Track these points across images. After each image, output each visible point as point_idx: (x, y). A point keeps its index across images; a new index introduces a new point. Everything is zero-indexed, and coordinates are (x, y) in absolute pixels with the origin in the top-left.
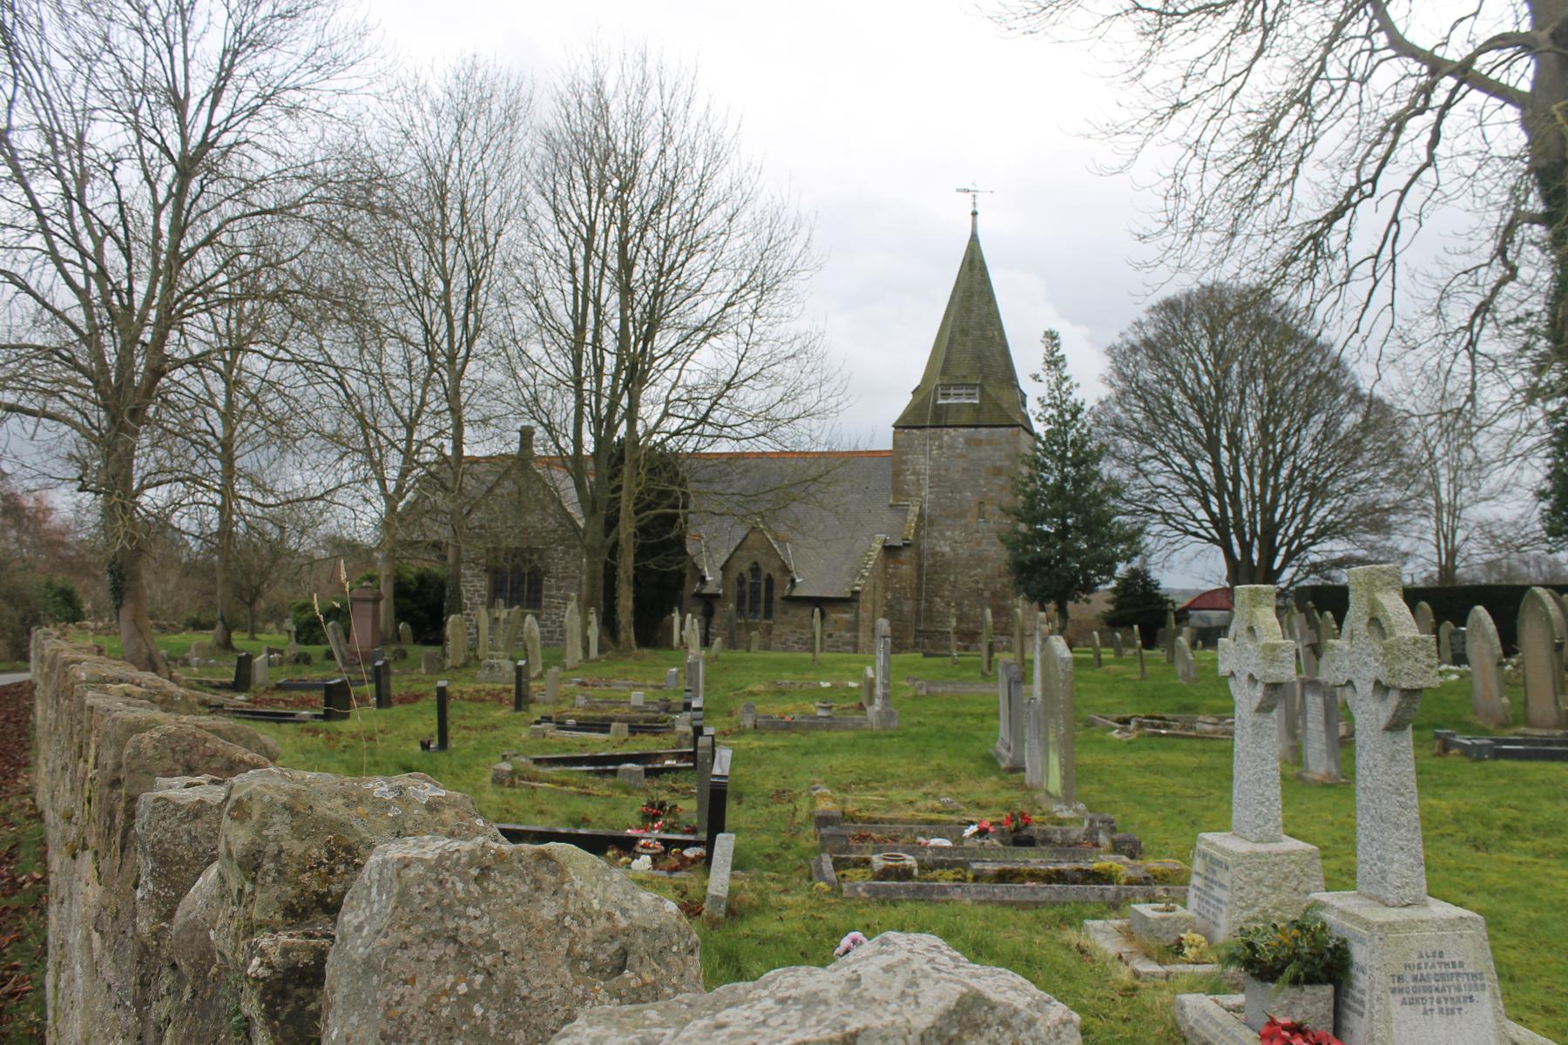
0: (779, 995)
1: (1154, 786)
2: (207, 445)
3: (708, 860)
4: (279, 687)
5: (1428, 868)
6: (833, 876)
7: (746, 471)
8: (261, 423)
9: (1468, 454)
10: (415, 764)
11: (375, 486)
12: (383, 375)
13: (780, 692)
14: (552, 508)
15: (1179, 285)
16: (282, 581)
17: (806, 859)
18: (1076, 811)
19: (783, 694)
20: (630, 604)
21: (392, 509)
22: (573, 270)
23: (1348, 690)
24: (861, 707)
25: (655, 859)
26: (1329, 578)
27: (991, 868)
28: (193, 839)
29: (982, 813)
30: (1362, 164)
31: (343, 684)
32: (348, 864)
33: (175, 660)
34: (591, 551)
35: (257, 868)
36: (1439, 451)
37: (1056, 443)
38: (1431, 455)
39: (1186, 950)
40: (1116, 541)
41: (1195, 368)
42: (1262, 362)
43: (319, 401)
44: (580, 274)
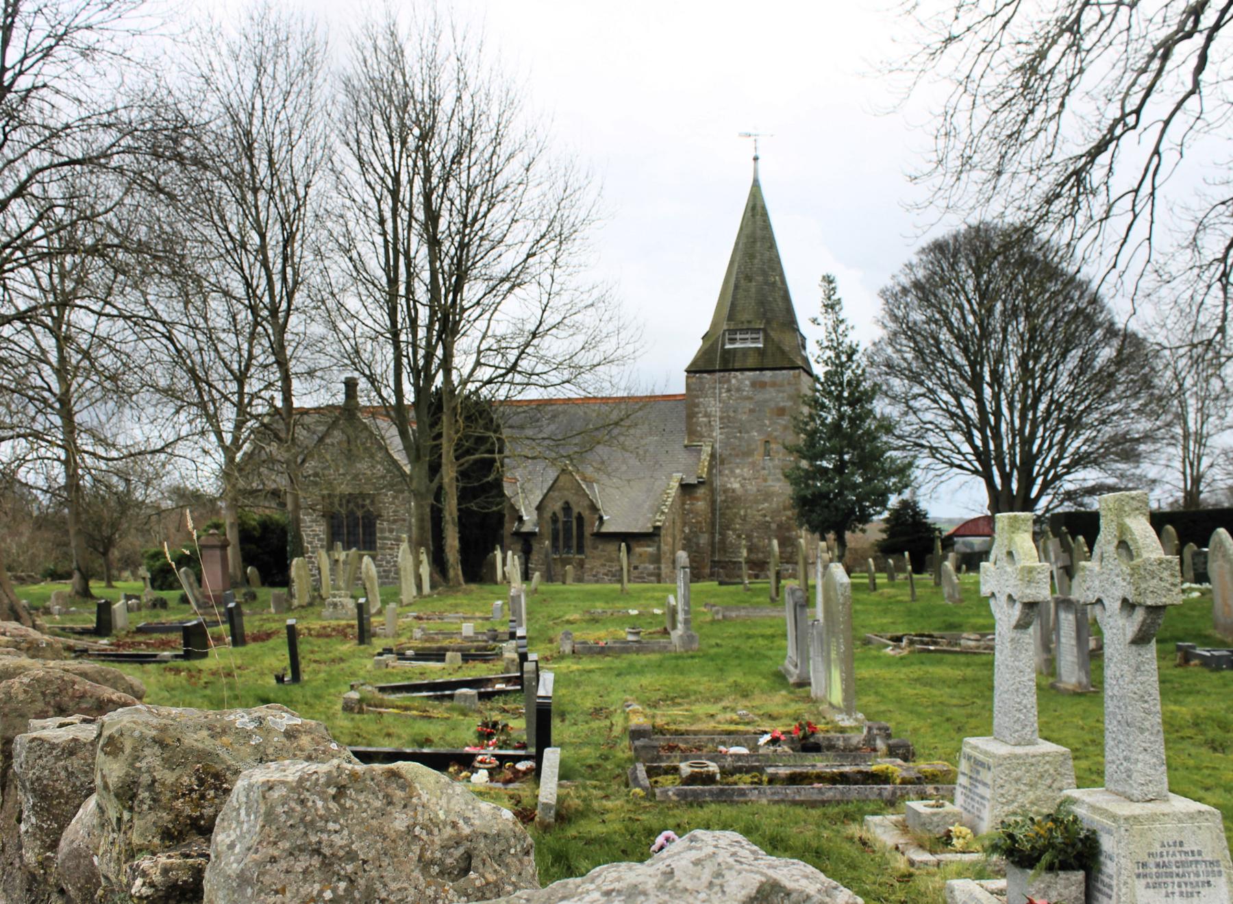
0: (605, 888)
1: (924, 697)
2: (44, 401)
3: (537, 772)
4: (140, 631)
5: (1169, 767)
6: (647, 782)
7: (554, 416)
8: (96, 378)
9: (1216, 384)
10: (272, 695)
11: (213, 437)
12: (209, 329)
13: (594, 621)
14: (380, 455)
15: (949, 226)
16: (133, 531)
17: (623, 768)
18: (856, 720)
19: (597, 621)
20: (456, 543)
21: (230, 460)
22: (382, 222)
23: (1098, 608)
24: (666, 632)
25: (491, 773)
26: (1081, 505)
27: (783, 771)
28: (70, 774)
29: (774, 723)
30: (1127, 94)
31: (199, 625)
32: (216, 789)
33: (37, 609)
34: (417, 494)
35: (133, 797)
36: (1188, 382)
37: (834, 383)
38: (1181, 386)
39: (955, 841)
40: (888, 474)
41: (961, 307)
42: (1024, 300)
43: (148, 352)
44: (389, 226)
